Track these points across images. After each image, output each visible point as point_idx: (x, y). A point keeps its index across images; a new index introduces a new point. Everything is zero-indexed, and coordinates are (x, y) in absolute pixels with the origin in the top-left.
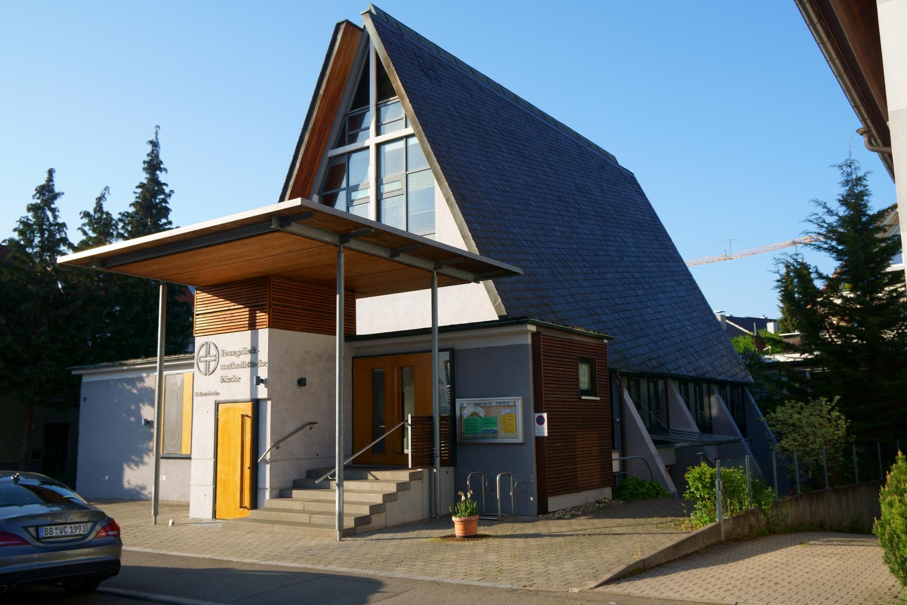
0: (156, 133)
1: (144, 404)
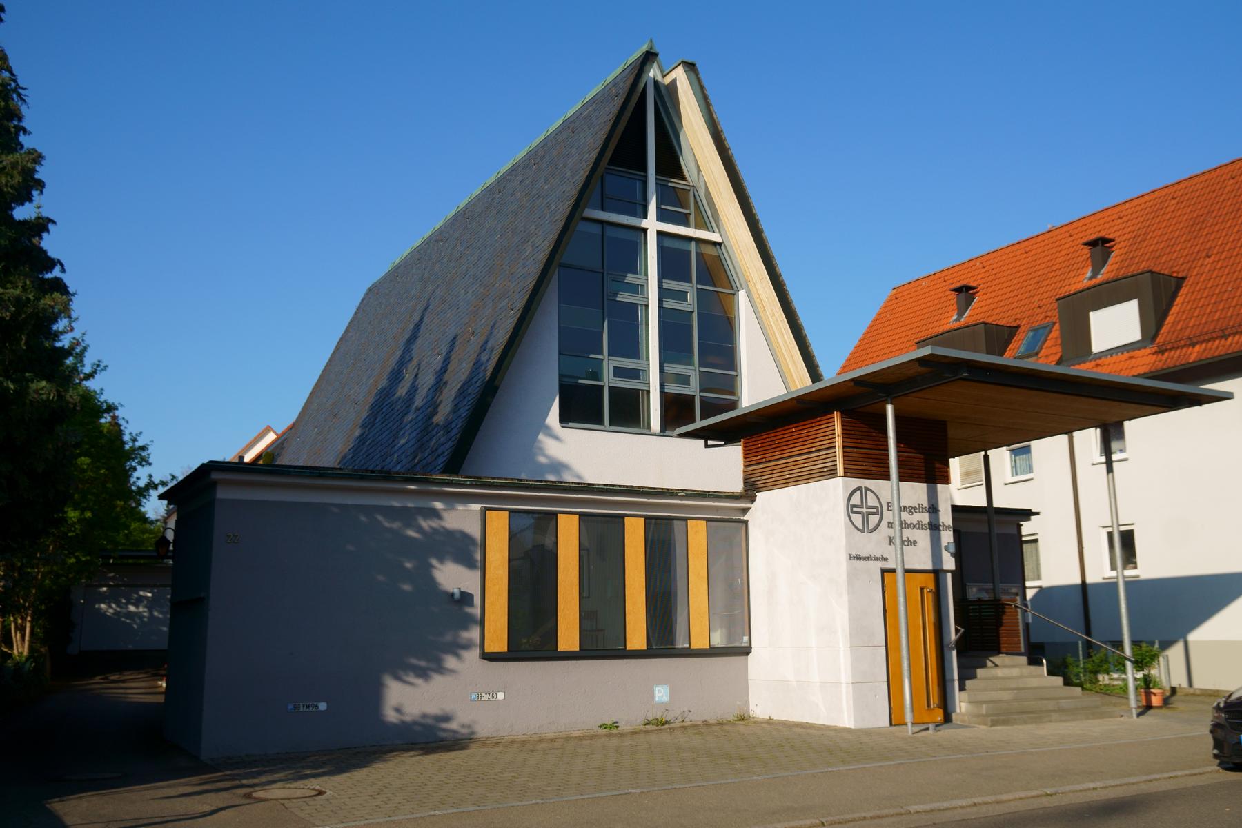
1: (441, 560)
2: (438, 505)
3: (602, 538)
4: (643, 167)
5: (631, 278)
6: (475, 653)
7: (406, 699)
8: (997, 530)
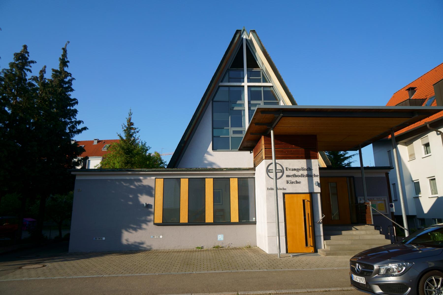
0: (66, 45)
1: (142, 194)
2: (141, 178)
3: (221, 186)
4: (243, 67)
5: (239, 102)
6: (152, 223)
7: (129, 237)
8: (365, 176)
